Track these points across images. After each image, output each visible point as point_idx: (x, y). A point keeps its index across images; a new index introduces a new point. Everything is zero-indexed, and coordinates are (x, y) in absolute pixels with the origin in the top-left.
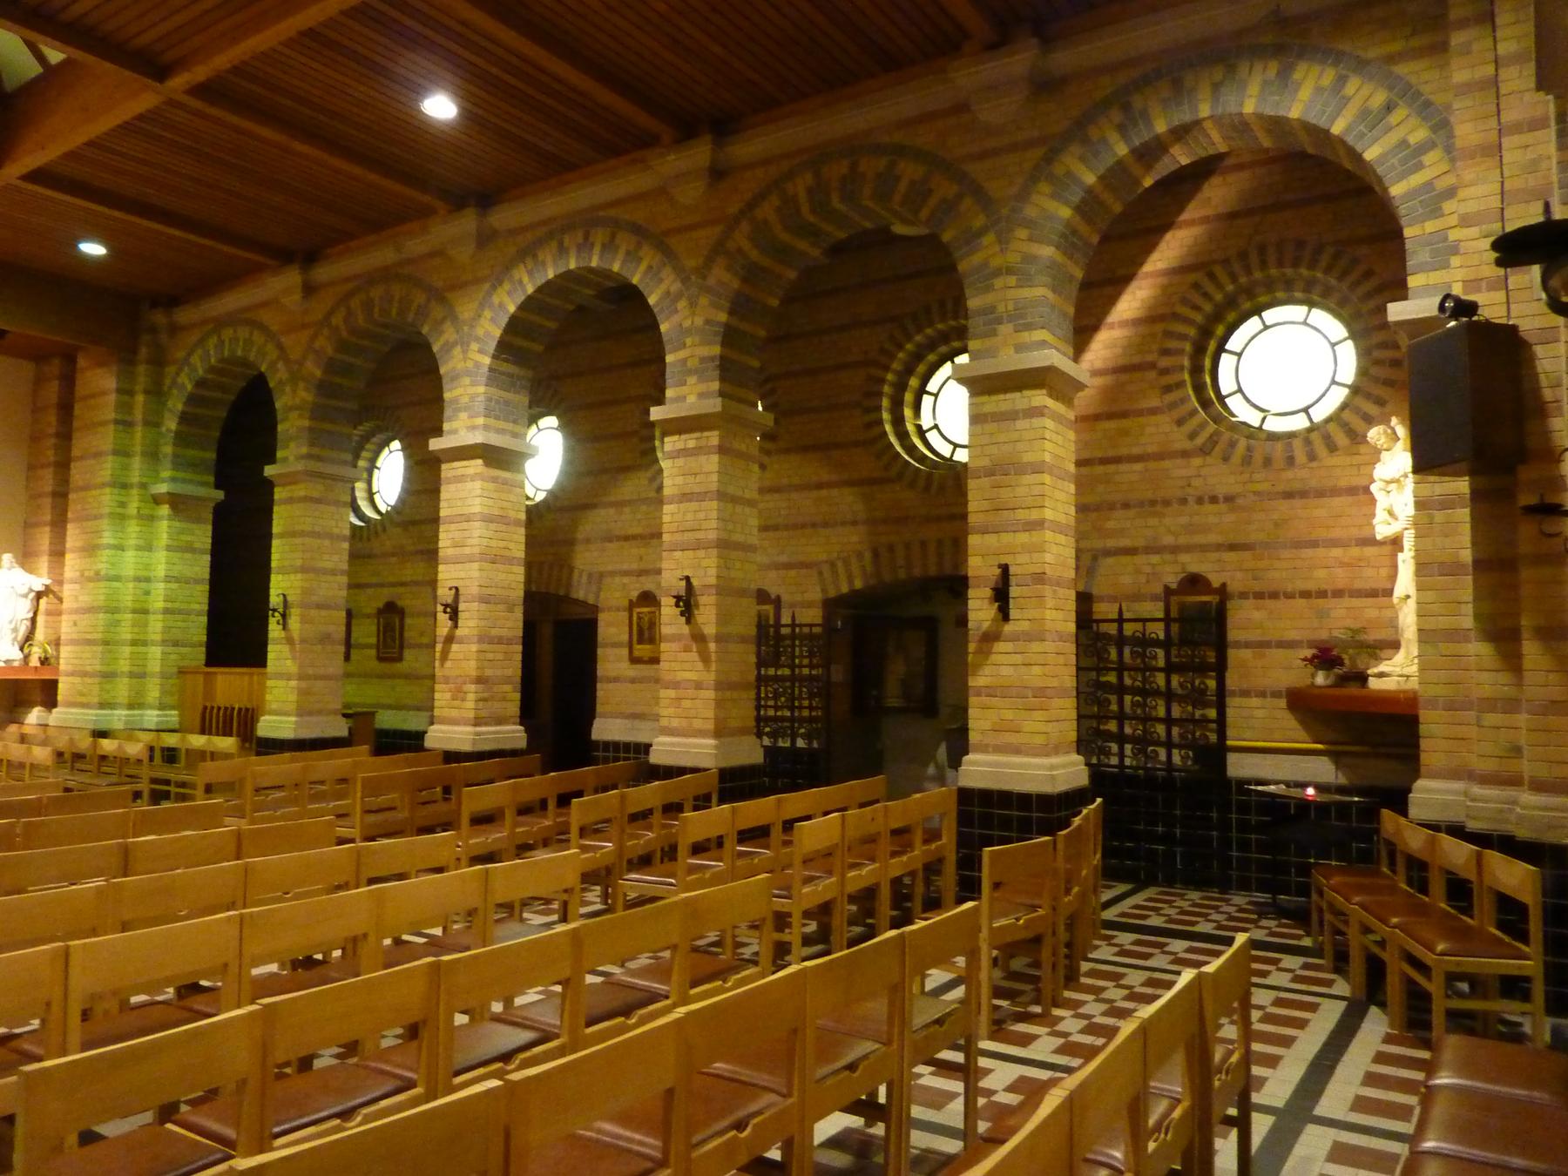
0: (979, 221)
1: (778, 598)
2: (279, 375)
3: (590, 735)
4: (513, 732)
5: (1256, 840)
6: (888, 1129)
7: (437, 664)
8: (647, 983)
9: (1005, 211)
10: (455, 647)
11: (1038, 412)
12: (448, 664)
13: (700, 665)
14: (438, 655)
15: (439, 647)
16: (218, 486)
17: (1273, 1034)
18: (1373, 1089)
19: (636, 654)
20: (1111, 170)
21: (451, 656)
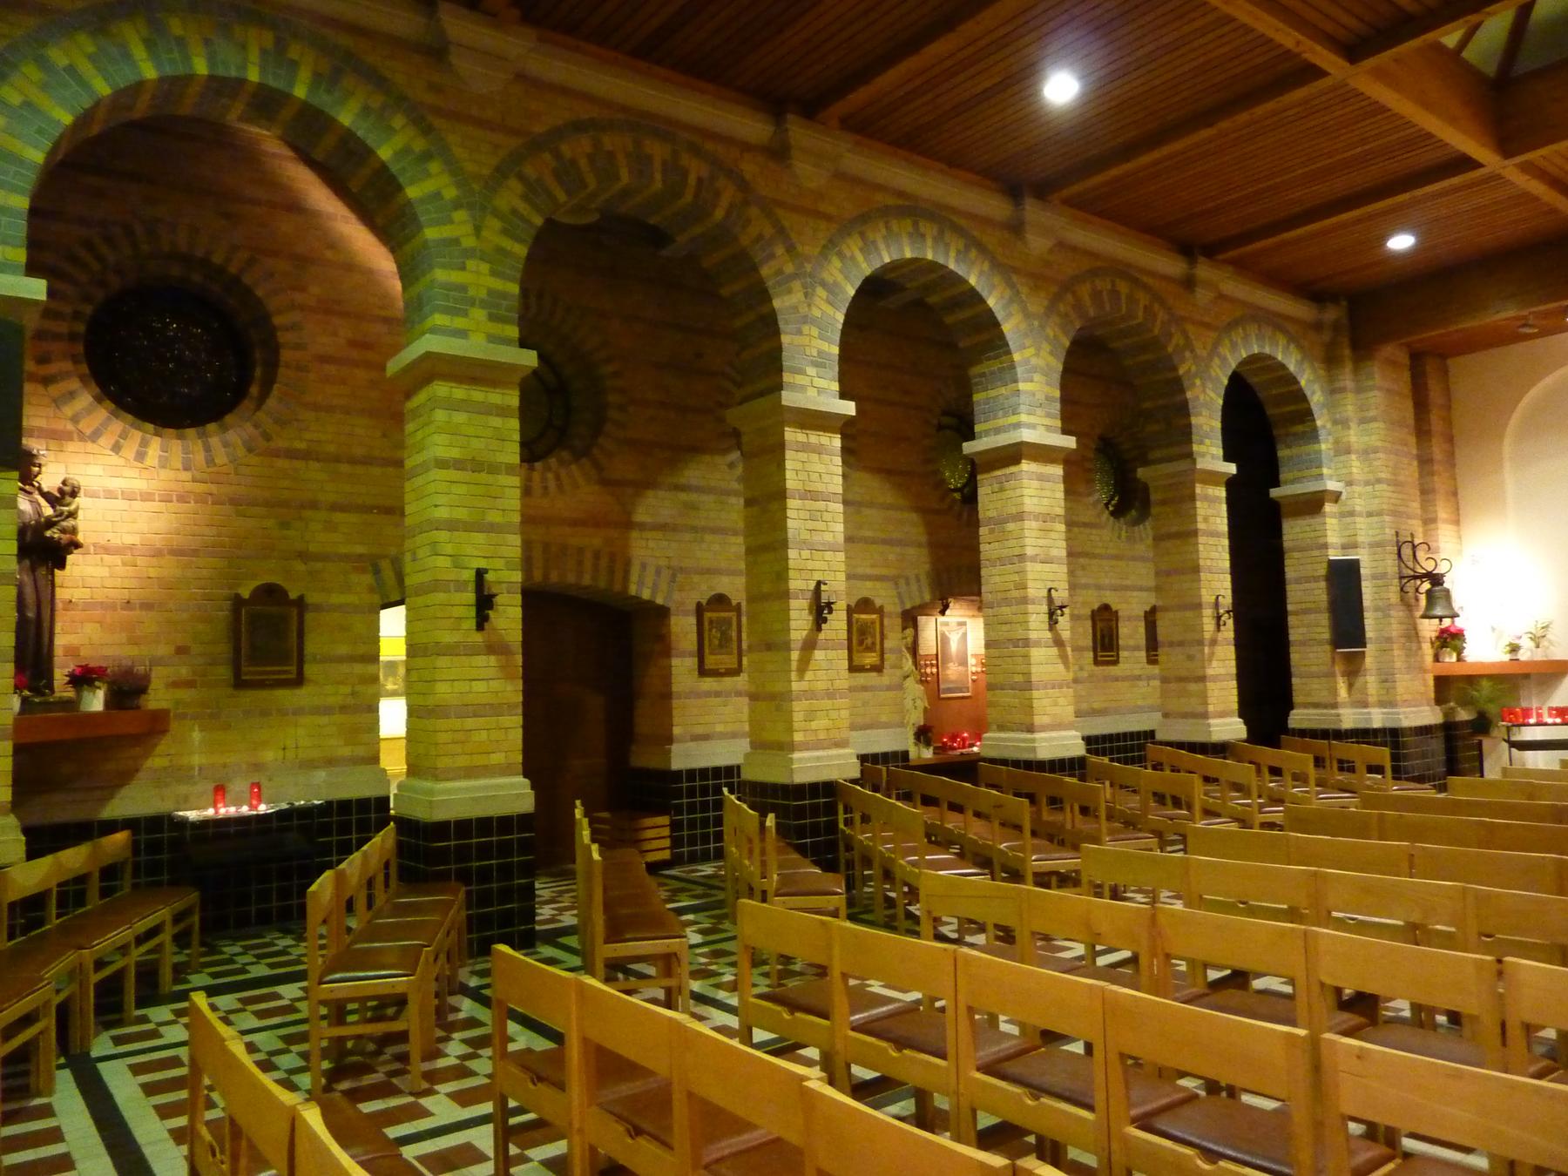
0: (789, 268)
1: (881, 608)
2: (1174, 341)
3: (1287, 723)
4: (512, 785)
5: (357, 833)
6: (1205, 976)
7: (794, 675)
8: (866, 1014)
9: (808, 267)
10: (818, 655)
11: (819, 450)
12: (809, 675)
13: (1061, 667)
14: (794, 665)
15: (795, 655)
16: (524, 343)
17: (150, 1062)
18: (170, 1094)
19: (856, 662)
20: (360, 142)
21: (812, 665)
